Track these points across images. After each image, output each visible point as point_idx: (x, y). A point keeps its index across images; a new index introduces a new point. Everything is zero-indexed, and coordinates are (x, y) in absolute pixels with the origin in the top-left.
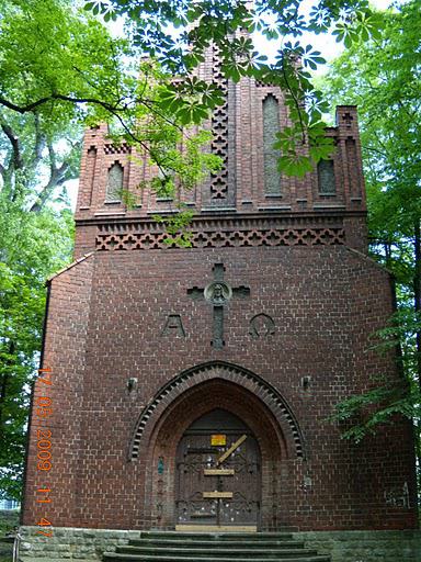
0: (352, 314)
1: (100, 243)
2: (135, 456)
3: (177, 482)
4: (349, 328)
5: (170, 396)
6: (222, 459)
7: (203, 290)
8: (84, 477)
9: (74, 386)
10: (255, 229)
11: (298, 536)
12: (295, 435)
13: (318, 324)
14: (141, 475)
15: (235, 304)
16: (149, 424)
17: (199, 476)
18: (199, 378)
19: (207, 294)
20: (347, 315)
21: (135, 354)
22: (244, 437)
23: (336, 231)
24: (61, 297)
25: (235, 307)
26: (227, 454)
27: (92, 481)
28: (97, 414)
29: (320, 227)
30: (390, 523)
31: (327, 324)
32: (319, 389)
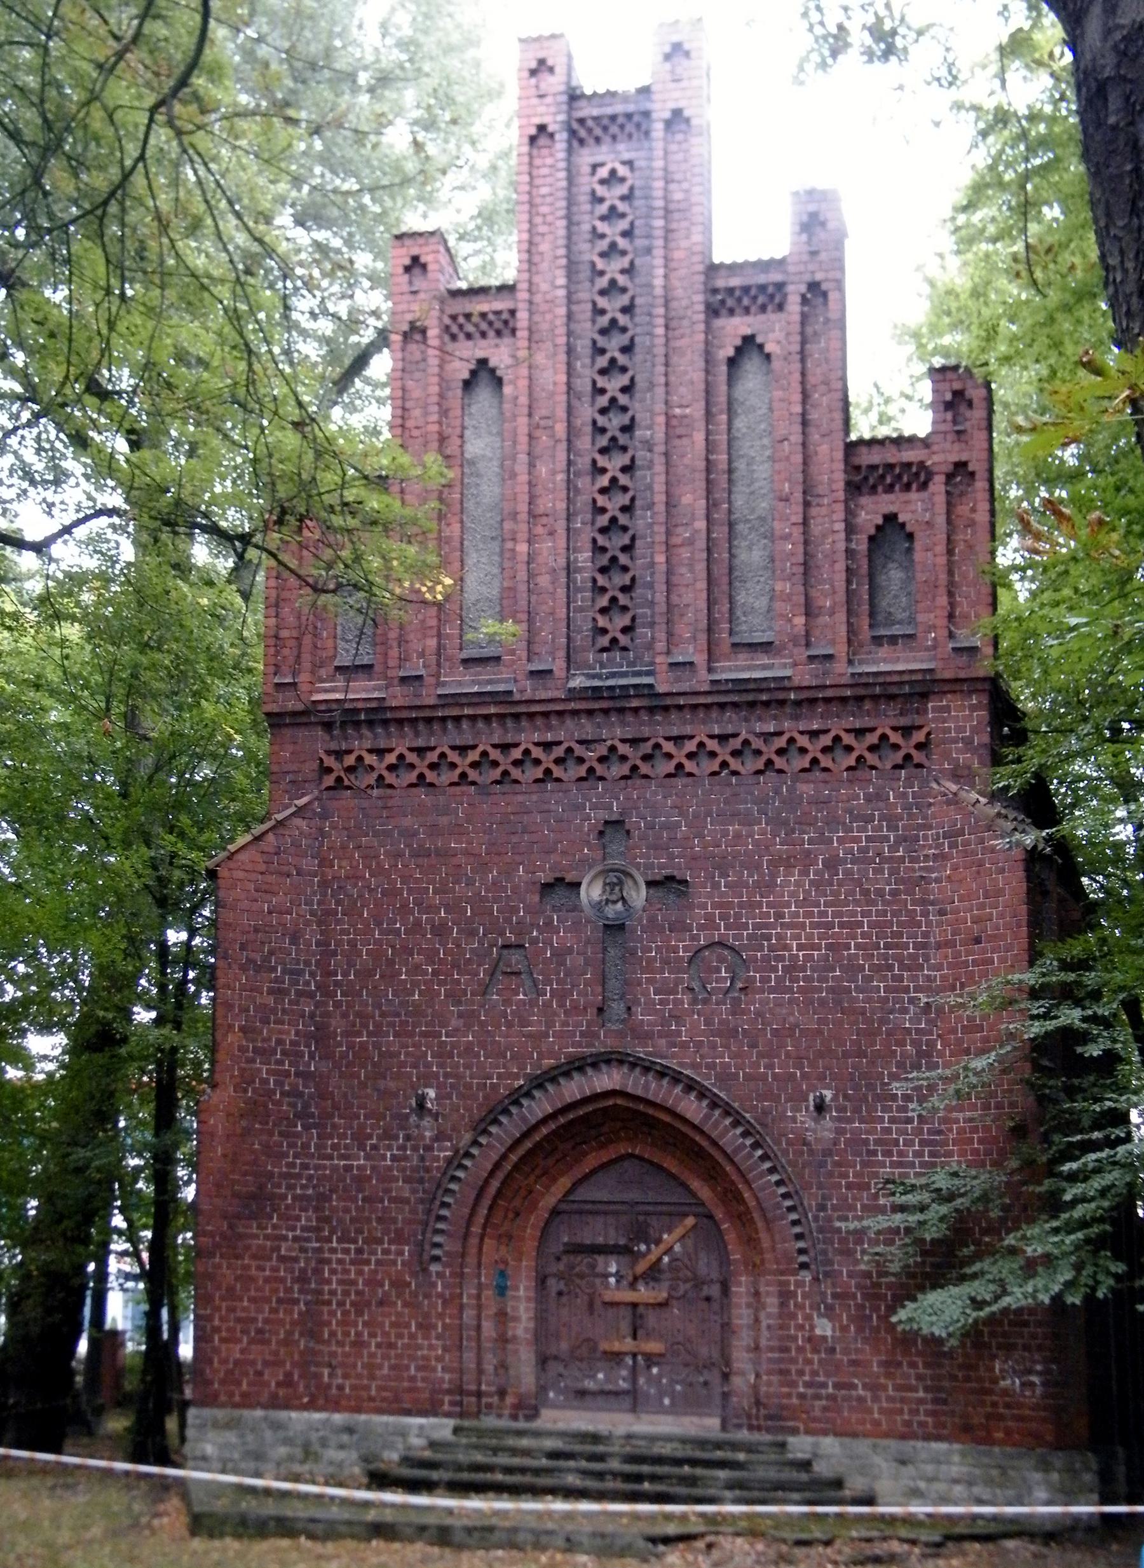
0: (939, 946)
1: (329, 770)
2: (436, 1259)
3: (541, 1318)
4: (928, 978)
5: (508, 1129)
6: (642, 1267)
7: (579, 884)
8: (329, 1303)
9: (293, 1105)
10: (701, 730)
11: (800, 1445)
12: (795, 1223)
13: (852, 969)
14: (453, 1301)
15: (652, 920)
16: (460, 1192)
17: (591, 1305)
18: (573, 1089)
19: (592, 892)
20: (924, 946)
21: (424, 1034)
22: (690, 1221)
23: (907, 731)
24: (245, 904)
25: (653, 926)
26: (652, 1257)
27: (345, 1313)
28: (347, 1169)
29: (867, 722)
30: (1008, 1432)
31: (876, 969)
32: (850, 1121)
